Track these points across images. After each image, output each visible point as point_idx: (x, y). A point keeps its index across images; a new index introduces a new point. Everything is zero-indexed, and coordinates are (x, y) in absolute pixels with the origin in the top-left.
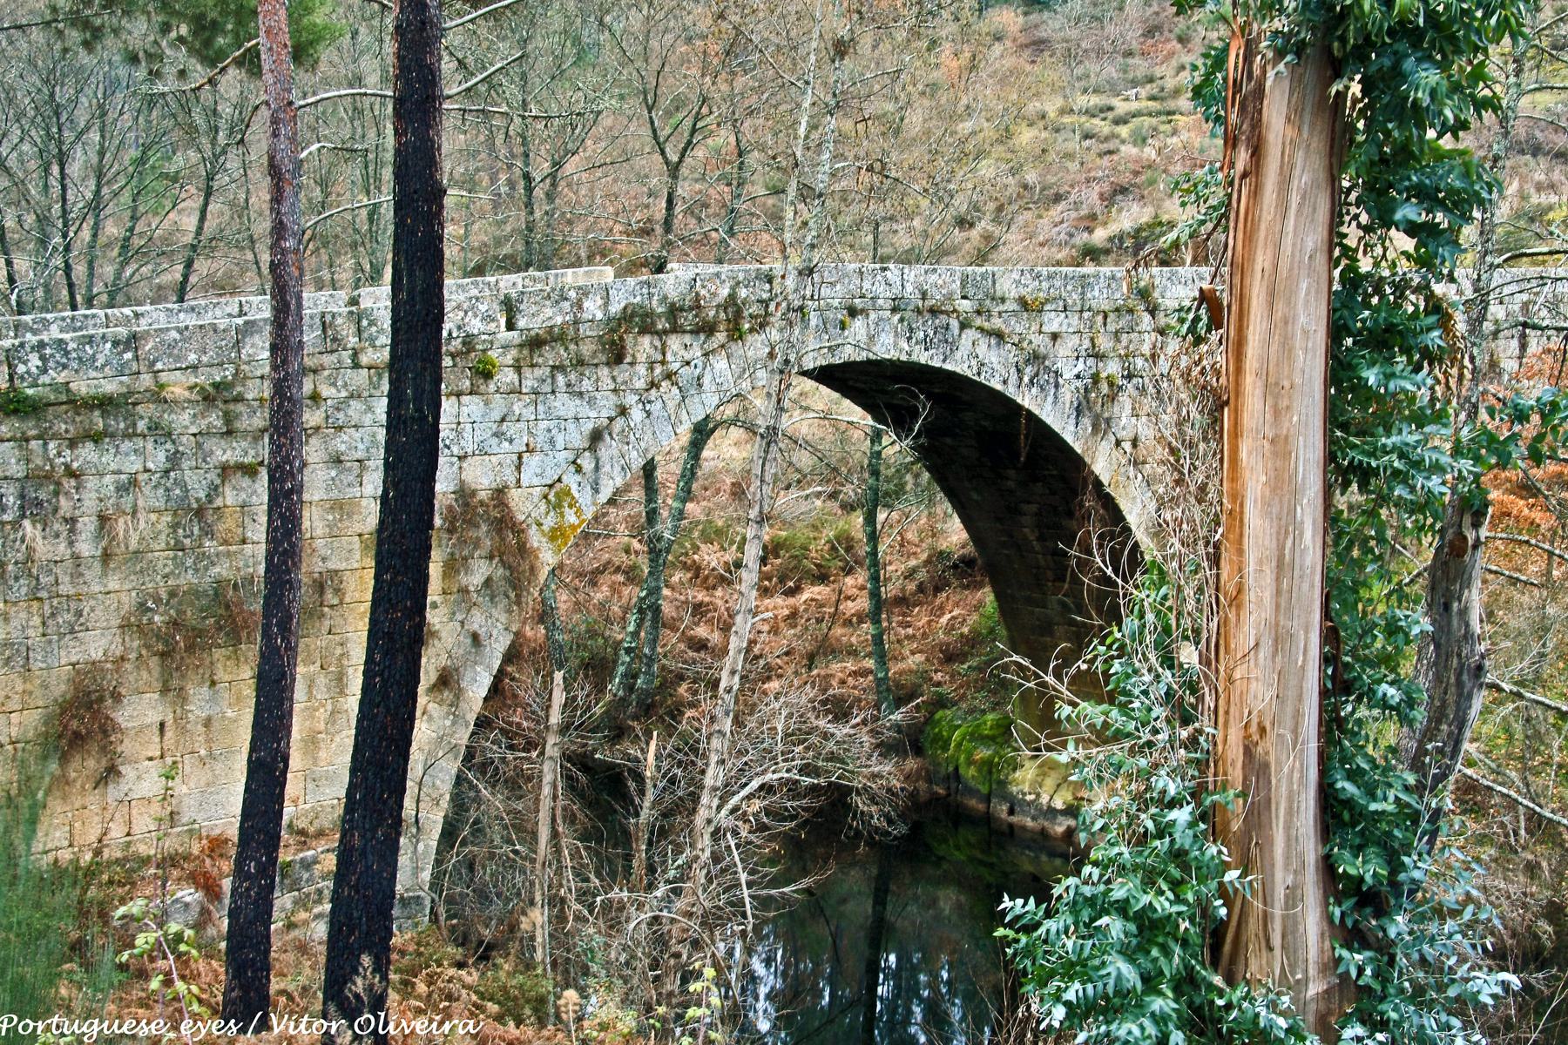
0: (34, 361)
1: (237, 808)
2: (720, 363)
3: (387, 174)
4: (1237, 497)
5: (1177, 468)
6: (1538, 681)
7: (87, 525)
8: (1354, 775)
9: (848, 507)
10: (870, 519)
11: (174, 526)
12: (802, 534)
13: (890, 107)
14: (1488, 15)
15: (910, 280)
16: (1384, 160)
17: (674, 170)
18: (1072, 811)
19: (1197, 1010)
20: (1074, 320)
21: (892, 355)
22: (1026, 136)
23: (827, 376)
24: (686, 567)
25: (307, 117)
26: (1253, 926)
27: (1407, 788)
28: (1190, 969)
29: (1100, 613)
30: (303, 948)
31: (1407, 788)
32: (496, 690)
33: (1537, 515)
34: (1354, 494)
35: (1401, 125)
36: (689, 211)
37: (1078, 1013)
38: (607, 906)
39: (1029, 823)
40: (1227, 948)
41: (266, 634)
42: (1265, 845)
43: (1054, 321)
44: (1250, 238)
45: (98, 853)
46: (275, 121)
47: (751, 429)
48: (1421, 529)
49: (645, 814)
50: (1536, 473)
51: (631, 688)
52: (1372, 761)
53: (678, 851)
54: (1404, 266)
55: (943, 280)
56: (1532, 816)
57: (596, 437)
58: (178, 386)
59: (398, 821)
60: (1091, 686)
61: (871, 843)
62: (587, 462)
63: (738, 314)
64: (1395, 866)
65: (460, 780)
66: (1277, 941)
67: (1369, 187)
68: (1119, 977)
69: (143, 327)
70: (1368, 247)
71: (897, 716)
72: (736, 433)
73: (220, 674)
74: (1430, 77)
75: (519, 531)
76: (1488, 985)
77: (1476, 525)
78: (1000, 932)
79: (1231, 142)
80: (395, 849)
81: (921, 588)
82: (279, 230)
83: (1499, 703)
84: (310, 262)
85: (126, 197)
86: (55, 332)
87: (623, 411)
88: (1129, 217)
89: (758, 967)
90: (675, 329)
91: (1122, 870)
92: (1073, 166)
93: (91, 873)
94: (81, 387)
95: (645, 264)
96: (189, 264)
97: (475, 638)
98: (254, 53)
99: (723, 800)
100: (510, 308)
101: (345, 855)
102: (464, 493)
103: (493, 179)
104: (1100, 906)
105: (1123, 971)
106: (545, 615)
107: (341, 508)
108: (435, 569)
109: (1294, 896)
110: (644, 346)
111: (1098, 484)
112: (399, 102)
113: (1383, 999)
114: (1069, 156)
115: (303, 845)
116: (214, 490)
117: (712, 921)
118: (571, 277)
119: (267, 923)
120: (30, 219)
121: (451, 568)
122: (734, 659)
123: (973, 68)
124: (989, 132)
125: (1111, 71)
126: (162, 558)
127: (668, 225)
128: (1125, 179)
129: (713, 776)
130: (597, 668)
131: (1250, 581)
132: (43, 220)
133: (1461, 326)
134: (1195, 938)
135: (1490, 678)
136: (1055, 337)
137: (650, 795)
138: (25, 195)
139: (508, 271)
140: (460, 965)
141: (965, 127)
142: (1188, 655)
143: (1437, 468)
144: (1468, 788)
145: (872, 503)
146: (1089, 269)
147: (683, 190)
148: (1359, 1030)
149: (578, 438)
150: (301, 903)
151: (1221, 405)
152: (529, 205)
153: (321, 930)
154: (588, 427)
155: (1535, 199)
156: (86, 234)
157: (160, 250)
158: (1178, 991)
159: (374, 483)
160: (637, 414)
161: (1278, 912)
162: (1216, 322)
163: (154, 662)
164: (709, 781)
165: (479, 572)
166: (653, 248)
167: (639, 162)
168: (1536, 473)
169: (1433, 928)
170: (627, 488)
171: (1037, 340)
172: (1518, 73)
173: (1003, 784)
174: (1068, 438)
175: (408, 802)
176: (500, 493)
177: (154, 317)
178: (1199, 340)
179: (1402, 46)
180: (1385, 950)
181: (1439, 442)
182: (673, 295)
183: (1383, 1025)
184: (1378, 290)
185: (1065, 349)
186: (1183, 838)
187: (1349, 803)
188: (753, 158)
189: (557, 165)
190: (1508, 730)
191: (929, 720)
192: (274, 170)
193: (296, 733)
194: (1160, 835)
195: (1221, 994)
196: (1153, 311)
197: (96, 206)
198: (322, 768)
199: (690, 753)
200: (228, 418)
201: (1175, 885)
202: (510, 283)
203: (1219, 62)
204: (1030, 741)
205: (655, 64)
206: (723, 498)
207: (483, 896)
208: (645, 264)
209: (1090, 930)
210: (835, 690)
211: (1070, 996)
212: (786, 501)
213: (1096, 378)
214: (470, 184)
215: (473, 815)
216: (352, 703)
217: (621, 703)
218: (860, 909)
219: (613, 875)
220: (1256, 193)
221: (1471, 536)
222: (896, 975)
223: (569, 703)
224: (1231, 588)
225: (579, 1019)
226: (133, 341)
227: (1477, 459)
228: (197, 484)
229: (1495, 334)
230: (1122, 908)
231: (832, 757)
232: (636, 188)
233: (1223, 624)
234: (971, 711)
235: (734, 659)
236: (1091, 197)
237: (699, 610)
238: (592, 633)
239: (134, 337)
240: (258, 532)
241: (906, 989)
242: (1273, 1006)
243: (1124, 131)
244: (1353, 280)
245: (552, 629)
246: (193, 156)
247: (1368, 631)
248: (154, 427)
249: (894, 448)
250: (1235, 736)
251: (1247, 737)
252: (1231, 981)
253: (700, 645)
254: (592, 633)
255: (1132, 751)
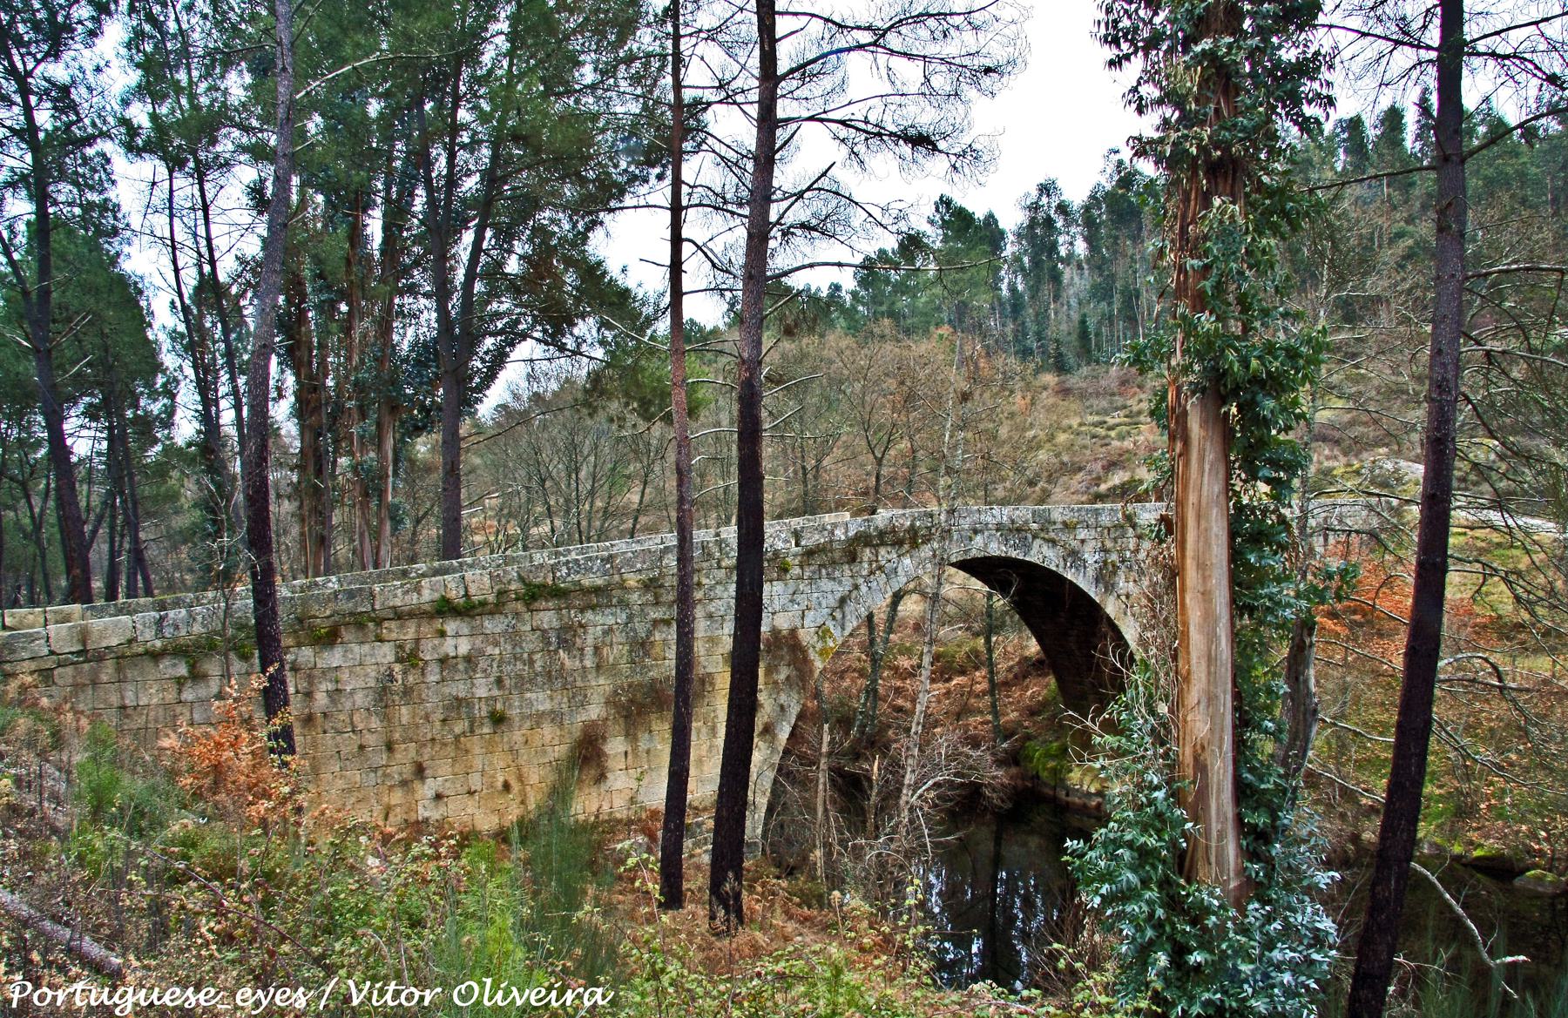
0: (565, 570)
1: (664, 795)
2: (907, 561)
3: (734, 469)
4: (1185, 624)
5: (1153, 610)
6: (1343, 716)
7: (589, 651)
8: (1252, 770)
9: (976, 635)
10: (988, 641)
11: (630, 652)
12: (952, 648)
13: (991, 425)
14: (1297, 373)
15: (1003, 514)
16: (1251, 446)
17: (879, 462)
18: (1100, 793)
19: (1172, 898)
20: (1093, 532)
21: (997, 553)
22: (1062, 438)
23: (963, 565)
24: (890, 668)
25: (693, 443)
26: (1200, 853)
27: (1280, 776)
28: (1167, 876)
29: (1113, 686)
30: (698, 867)
31: (1280, 776)
32: (792, 734)
33: (1338, 628)
34: (1246, 620)
35: (1258, 428)
36: (887, 482)
37: (1107, 900)
38: (854, 846)
39: (1077, 800)
40: (1187, 863)
41: (677, 707)
42: (1207, 808)
43: (1082, 534)
44: (1185, 487)
45: (597, 817)
46: (679, 446)
47: (923, 594)
48: (1281, 638)
49: (873, 798)
50: (1339, 606)
51: (863, 733)
52: (1261, 762)
53: (890, 819)
54: (1265, 500)
55: (1023, 513)
56: (1342, 788)
57: (843, 601)
58: (632, 580)
59: (745, 803)
60: (1111, 727)
61: (993, 813)
62: (838, 615)
63: (916, 533)
64: (1275, 818)
65: (775, 781)
66: (1213, 859)
67: (1245, 460)
68: (1128, 881)
69: (614, 551)
70: (1246, 491)
71: (1005, 745)
72: (915, 597)
73: (654, 727)
74: (1270, 404)
75: (804, 651)
76: (1323, 878)
77: (1310, 635)
78: (1065, 858)
79: (1172, 438)
80: (744, 817)
81: (1016, 677)
82: (681, 500)
83: (1323, 729)
84: (696, 516)
85: (606, 487)
86: (573, 556)
87: (856, 587)
88: (1118, 478)
89: (932, 878)
90: (883, 544)
91: (1130, 824)
92: (1088, 452)
93: (595, 826)
94: (586, 582)
95: (865, 510)
96: (636, 519)
97: (782, 707)
98: (669, 414)
99: (914, 792)
100: (797, 535)
101: (718, 820)
102: (775, 632)
103: (786, 470)
104: (1117, 843)
105: (1130, 876)
106: (817, 695)
107: (713, 641)
108: (761, 672)
109: (1221, 835)
110: (867, 553)
111: (1108, 618)
112: (740, 434)
113: (1269, 888)
114: (1085, 447)
115: (697, 815)
116: (650, 633)
117: (909, 855)
118: (828, 518)
119: (681, 853)
120: (561, 500)
121: (769, 672)
122: (918, 716)
123: (1033, 404)
124: (1042, 435)
125: (1104, 404)
126: (624, 667)
127: (877, 490)
128: (1115, 458)
129: (909, 778)
130: (844, 722)
131: (1194, 668)
132: (567, 501)
133: (1296, 532)
134: (1169, 860)
135: (1320, 716)
136: (1083, 541)
137: (875, 790)
138: (559, 489)
139: (794, 516)
140: (778, 878)
141: (1030, 434)
142: (1163, 709)
143: (1289, 605)
144: (1310, 774)
145: (989, 631)
146: (1099, 506)
147: (884, 471)
148: (1257, 905)
149: (832, 601)
150: (696, 845)
151: (1174, 576)
152: (805, 482)
153: (706, 859)
154: (838, 596)
155: (1326, 464)
156: (587, 507)
157: (622, 513)
158: (1161, 886)
159: (729, 627)
160: (864, 589)
161: (1213, 844)
162: (1169, 531)
163: (621, 721)
164: (906, 782)
165: (782, 676)
166: (869, 502)
167: (861, 458)
168: (1339, 606)
169: (1294, 850)
170: (859, 627)
171: (1074, 543)
172: (1313, 400)
173: (1063, 780)
174: (1092, 595)
175: (750, 793)
176: (793, 631)
177: (621, 546)
178: (1161, 542)
179: (1256, 388)
180: (1269, 863)
181: (1289, 591)
182: (881, 526)
183: (1270, 902)
184: (1253, 513)
185: (1089, 547)
186: (1162, 807)
187: (1250, 785)
188: (921, 454)
189: (819, 461)
190: (1329, 743)
191: (1022, 747)
192: (679, 471)
193: (692, 758)
194: (1150, 805)
195: (1184, 888)
196: (1134, 526)
197: (592, 493)
198: (706, 775)
199: (895, 768)
200: (656, 596)
201: (1159, 832)
202: (796, 522)
203: (1163, 398)
204: (1080, 757)
205: (868, 409)
206: (909, 631)
207: (789, 842)
208: (865, 510)
209: (1114, 857)
210: (972, 732)
211: (1103, 891)
212: (943, 632)
213: (1105, 562)
214: (775, 473)
215: (782, 800)
216: (720, 741)
217: (858, 741)
218: (987, 847)
219: (857, 832)
220: (1187, 465)
221: (1307, 641)
222: (1005, 882)
223: (832, 742)
224: (1184, 672)
225: (841, 906)
226: (610, 558)
227: (1309, 600)
228: (641, 629)
229: (1311, 535)
230: (1130, 845)
231: (971, 768)
232: (859, 472)
233: (1181, 692)
234: (1045, 742)
235: (918, 716)
236: (1098, 467)
237: (898, 691)
238: (842, 704)
239: (611, 556)
240: (672, 654)
241: (1011, 890)
242: (1211, 894)
243: (1113, 434)
244: (1240, 508)
245: (821, 702)
246: (639, 465)
247: (1256, 692)
248: (621, 602)
249: (999, 602)
250: (1188, 751)
251: (1195, 751)
252: (1189, 882)
253: (900, 709)
254: (842, 704)
255: (1134, 761)
